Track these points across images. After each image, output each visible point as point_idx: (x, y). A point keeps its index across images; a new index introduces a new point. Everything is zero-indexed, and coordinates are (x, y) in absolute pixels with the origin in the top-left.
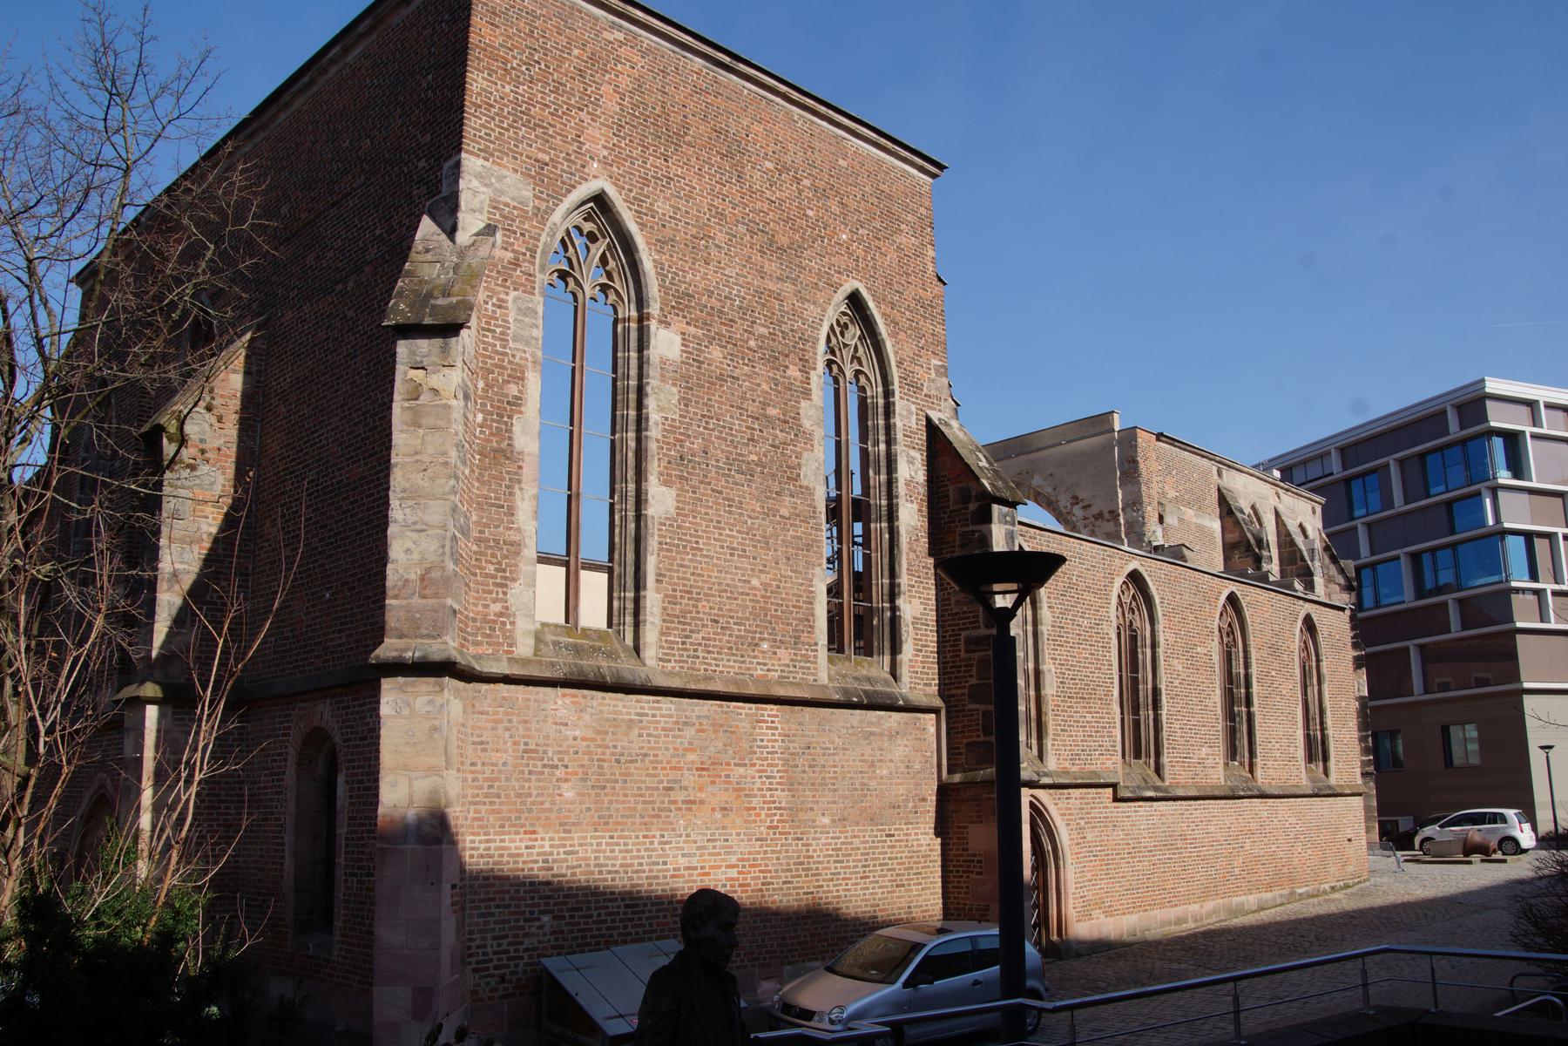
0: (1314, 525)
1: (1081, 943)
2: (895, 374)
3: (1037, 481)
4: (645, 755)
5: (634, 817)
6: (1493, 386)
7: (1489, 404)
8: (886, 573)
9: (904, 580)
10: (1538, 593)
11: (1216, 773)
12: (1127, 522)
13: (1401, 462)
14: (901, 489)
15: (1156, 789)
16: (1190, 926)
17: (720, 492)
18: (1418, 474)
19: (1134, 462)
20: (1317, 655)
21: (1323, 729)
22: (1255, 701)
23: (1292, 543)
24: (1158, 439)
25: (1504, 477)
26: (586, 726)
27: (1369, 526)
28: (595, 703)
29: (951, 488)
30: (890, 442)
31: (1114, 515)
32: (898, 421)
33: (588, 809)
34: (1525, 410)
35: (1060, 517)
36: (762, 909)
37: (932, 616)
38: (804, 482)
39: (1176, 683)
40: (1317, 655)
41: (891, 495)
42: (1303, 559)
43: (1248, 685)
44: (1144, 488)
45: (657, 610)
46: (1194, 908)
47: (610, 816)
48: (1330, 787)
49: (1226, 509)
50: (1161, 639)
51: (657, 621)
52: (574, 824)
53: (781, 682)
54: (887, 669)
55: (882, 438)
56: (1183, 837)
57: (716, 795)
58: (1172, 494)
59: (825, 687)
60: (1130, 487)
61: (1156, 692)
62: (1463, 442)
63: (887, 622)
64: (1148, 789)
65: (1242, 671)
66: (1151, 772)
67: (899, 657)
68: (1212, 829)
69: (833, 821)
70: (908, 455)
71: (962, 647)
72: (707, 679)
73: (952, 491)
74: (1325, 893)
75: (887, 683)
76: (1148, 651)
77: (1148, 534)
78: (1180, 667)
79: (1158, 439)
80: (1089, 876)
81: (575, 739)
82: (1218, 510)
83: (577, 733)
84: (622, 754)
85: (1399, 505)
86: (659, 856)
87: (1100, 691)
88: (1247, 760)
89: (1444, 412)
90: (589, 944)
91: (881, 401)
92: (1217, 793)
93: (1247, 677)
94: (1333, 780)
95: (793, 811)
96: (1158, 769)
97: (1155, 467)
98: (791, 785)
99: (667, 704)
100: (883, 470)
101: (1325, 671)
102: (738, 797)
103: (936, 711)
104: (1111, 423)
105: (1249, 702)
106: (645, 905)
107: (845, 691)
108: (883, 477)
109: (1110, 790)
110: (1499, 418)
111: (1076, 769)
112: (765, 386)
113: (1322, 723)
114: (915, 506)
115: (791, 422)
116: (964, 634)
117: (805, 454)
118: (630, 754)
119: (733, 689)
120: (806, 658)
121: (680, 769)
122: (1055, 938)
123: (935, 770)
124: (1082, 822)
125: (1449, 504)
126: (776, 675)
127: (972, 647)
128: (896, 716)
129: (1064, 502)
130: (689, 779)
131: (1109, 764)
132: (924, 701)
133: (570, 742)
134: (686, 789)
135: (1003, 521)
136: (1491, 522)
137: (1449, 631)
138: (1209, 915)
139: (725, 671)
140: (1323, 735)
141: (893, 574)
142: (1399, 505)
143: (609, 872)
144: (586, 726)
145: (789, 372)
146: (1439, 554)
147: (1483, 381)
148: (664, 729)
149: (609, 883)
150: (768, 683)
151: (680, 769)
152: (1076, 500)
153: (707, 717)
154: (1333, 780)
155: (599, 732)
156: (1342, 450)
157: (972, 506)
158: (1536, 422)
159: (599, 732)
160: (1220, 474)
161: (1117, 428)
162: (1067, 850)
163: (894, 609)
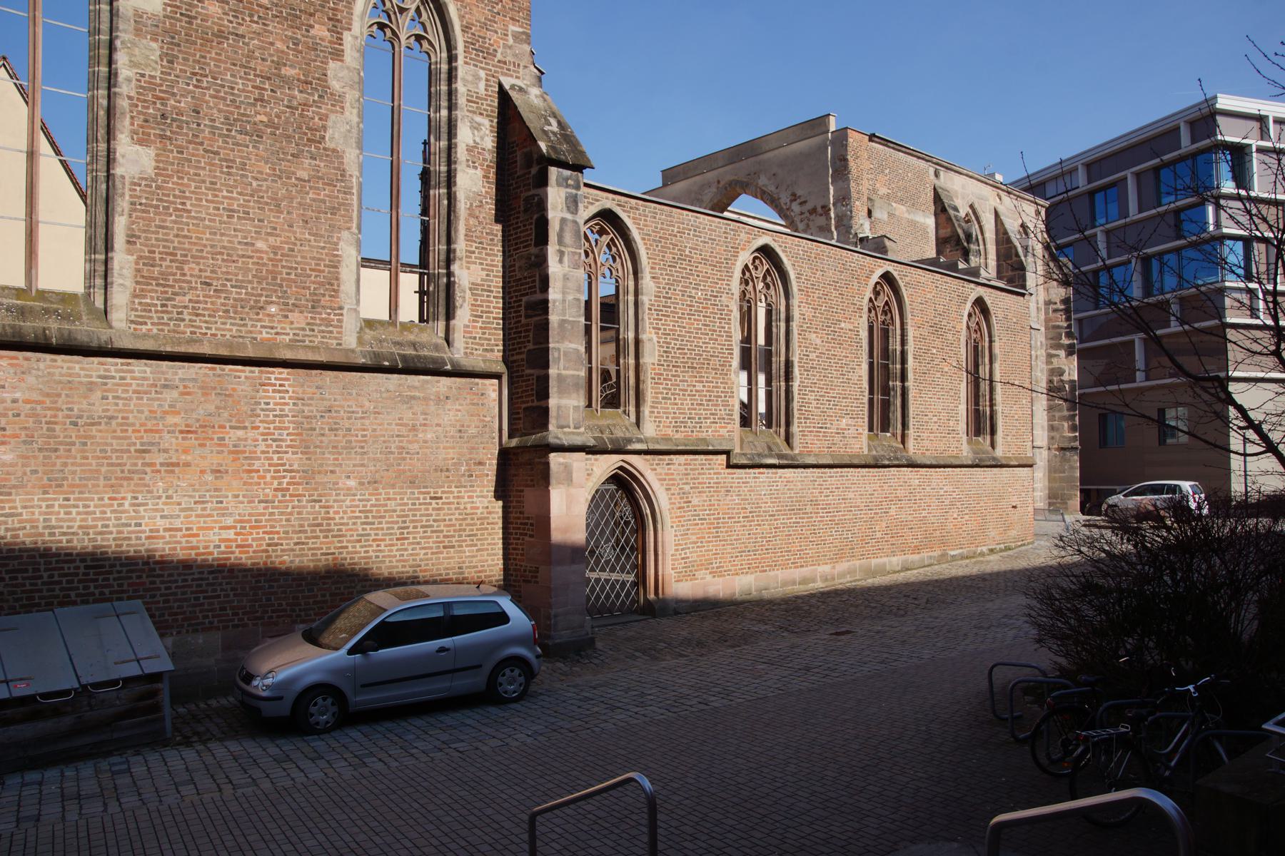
0: (1037, 225)
1: (679, 601)
2: (460, 39)
3: (763, 181)
4: (111, 418)
5: (98, 479)
6: (1224, 102)
7: (1219, 119)
8: (444, 239)
9: (460, 246)
10: (1251, 292)
11: (859, 441)
12: (837, 216)
13: (1137, 175)
14: (461, 154)
15: (780, 456)
16: (819, 585)
17: (217, 153)
18: (1153, 184)
19: (844, 160)
20: (990, 336)
21: (992, 406)
22: (910, 375)
23: (1009, 240)
24: (870, 140)
25: (1228, 187)
26: (31, 389)
27: (1108, 233)
28: (42, 365)
29: (519, 153)
30: (451, 107)
31: (826, 209)
32: (460, 87)
33: (36, 472)
34: (1256, 125)
35: (782, 213)
36: (267, 569)
37: (498, 282)
38: (329, 144)
39: (813, 356)
40: (990, 336)
41: (450, 161)
42: (1017, 255)
43: (904, 361)
44: (852, 184)
45: (128, 272)
46: (826, 569)
47: (65, 479)
48: (994, 459)
49: (941, 207)
50: (796, 313)
51: (129, 283)
52: (14, 487)
53: (291, 346)
54: (442, 334)
55: (444, 103)
56: (815, 503)
57: (208, 457)
58: (883, 191)
59: (353, 351)
60: (840, 183)
61: (789, 364)
62: (1194, 155)
63: (442, 288)
64: (771, 456)
65: (899, 348)
66: (780, 441)
67: (452, 322)
68: (851, 495)
69: (361, 484)
70: (472, 121)
71: (523, 313)
72: (191, 341)
73: (519, 156)
74: (982, 554)
75: (437, 347)
76: (783, 325)
77: (855, 227)
78: (818, 341)
79: (870, 140)
80: (694, 538)
81: (15, 401)
82: (933, 208)
83: (18, 395)
84: (81, 417)
85: (1134, 214)
86: (131, 518)
87: (715, 362)
88: (899, 432)
89: (1177, 129)
90: (39, 605)
91: (445, 67)
92: (856, 462)
93: (903, 353)
94: (999, 452)
95: (308, 475)
96: (788, 439)
97: (866, 165)
98: (306, 449)
99: (138, 366)
100: (444, 136)
101: (997, 351)
102: (235, 460)
103: (497, 376)
104: (827, 125)
105: (904, 378)
106: (113, 566)
107: (376, 355)
108: (444, 143)
109: (724, 457)
110: (1230, 133)
111: (679, 437)
112: (279, 45)
113: (991, 399)
114: (479, 173)
115: (316, 83)
116: (524, 299)
117: (333, 117)
118: (91, 417)
119: (224, 352)
120: (328, 322)
121: (157, 431)
122: (652, 596)
123: (496, 435)
124: (687, 488)
125: (1178, 212)
126: (287, 338)
127: (530, 312)
128: (445, 381)
129: (784, 199)
130: (169, 441)
131: (723, 432)
132: (480, 366)
133: (9, 404)
134: (166, 451)
135: (563, 183)
136: (1211, 228)
137: (1169, 326)
138: (842, 575)
139: (219, 333)
140: (992, 411)
141: (449, 241)
142: (1134, 214)
143: (64, 534)
144: (31, 389)
145: (312, 32)
146: (1166, 257)
147: (1215, 97)
148: (135, 392)
149: (64, 544)
150: (274, 345)
151: (157, 431)
152: (794, 197)
153: (195, 380)
154: (999, 452)
155: (48, 395)
156: (1088, 166)
157: (534, 170)
158: (1264, 134)
159: (48, 395)
160: (937, 175)
161: (832, 128)
162: (666, 514)
163: (449, 274)
